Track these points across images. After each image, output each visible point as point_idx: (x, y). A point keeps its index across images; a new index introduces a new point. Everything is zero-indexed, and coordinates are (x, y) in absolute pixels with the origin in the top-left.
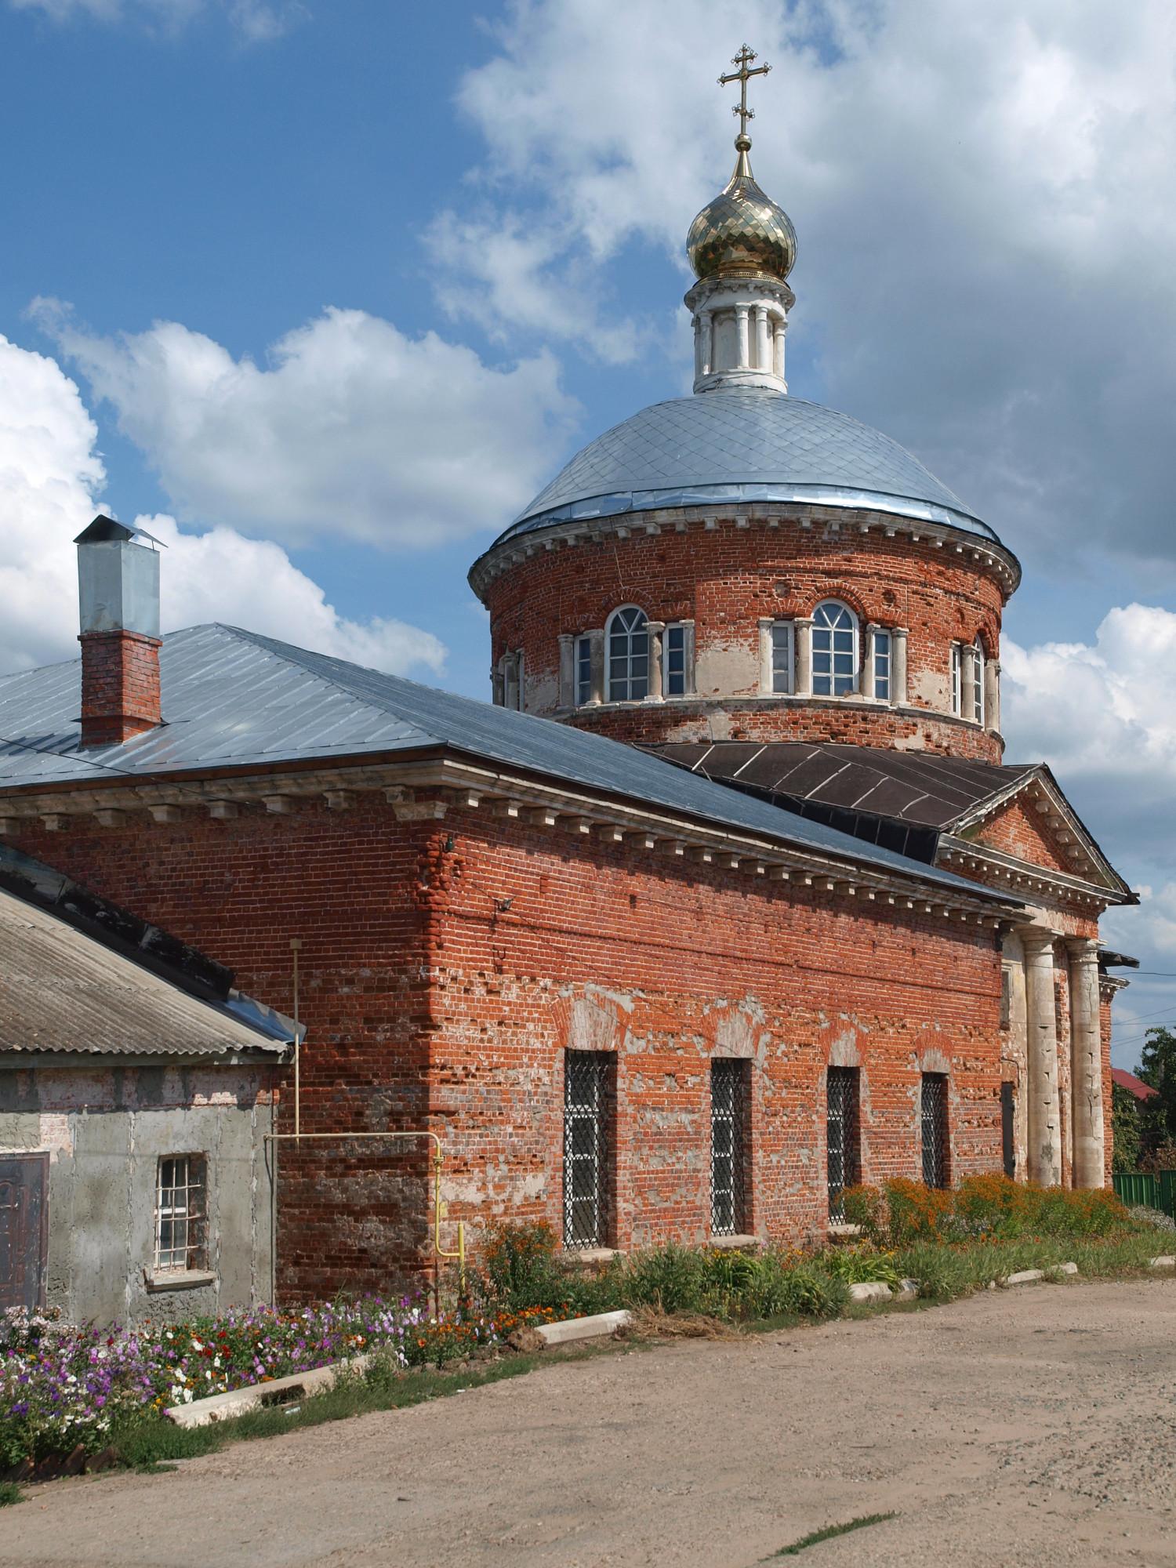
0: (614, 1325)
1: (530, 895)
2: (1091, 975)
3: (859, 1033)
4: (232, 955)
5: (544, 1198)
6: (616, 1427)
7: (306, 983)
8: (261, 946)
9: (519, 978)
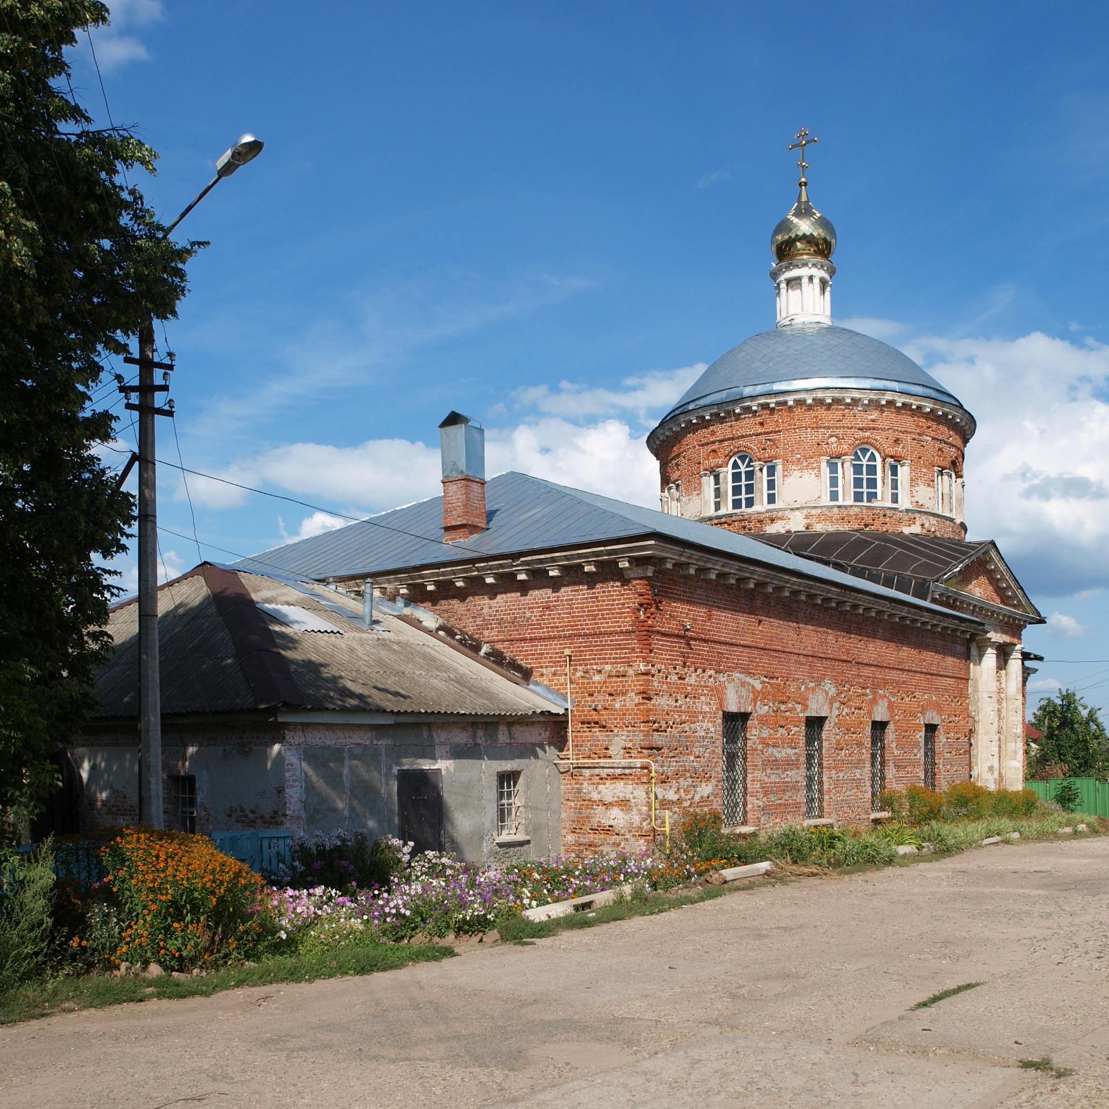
0: (764, 870)
1: (702, 621)
2: (1015, 664)
3: (890, 701)
4: (532, 659)
5: (712, 798)
6: (785, 929)
7: (574, 674)
8: (548, 654)
9: (696, 671)
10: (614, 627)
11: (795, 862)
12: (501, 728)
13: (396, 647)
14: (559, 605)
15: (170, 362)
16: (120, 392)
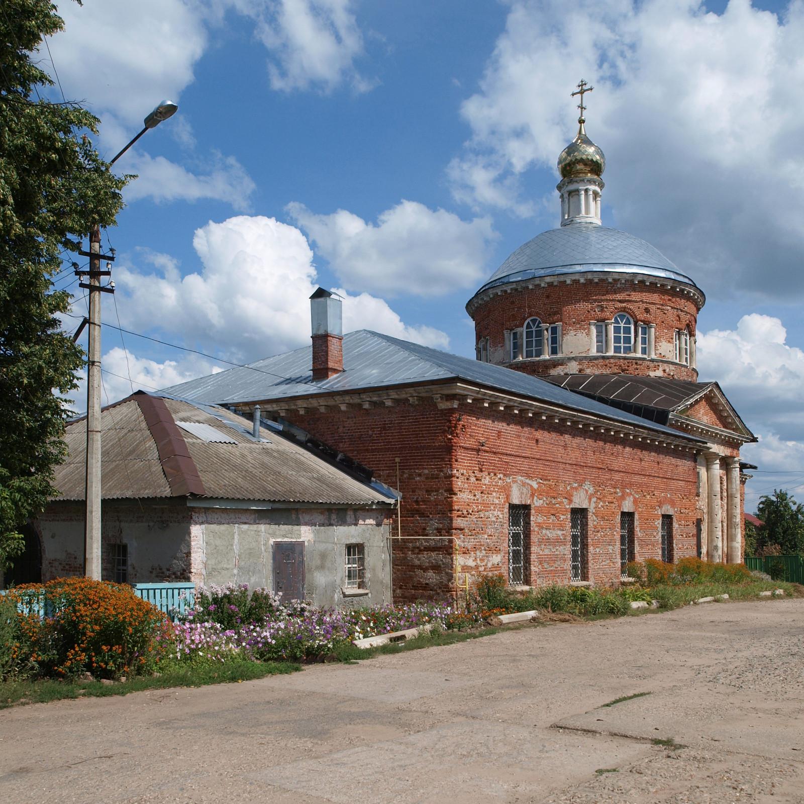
0: (531, 616)
1: (494, 439)
3: (634, 498)
4: (372, 464)
5: (500, 565)
6: (533, 656)
9: (489, 474)
10: (430, 443)
11: (554, 611)
12: (349, 513)
13: (275, 454)
14: (392, 427)
15: (111, 255)
16: (76, 275)
